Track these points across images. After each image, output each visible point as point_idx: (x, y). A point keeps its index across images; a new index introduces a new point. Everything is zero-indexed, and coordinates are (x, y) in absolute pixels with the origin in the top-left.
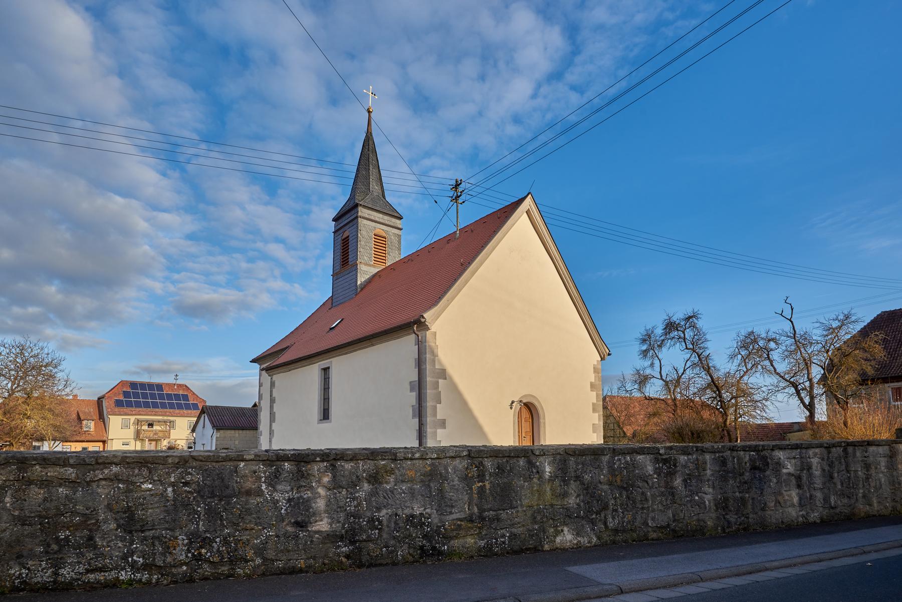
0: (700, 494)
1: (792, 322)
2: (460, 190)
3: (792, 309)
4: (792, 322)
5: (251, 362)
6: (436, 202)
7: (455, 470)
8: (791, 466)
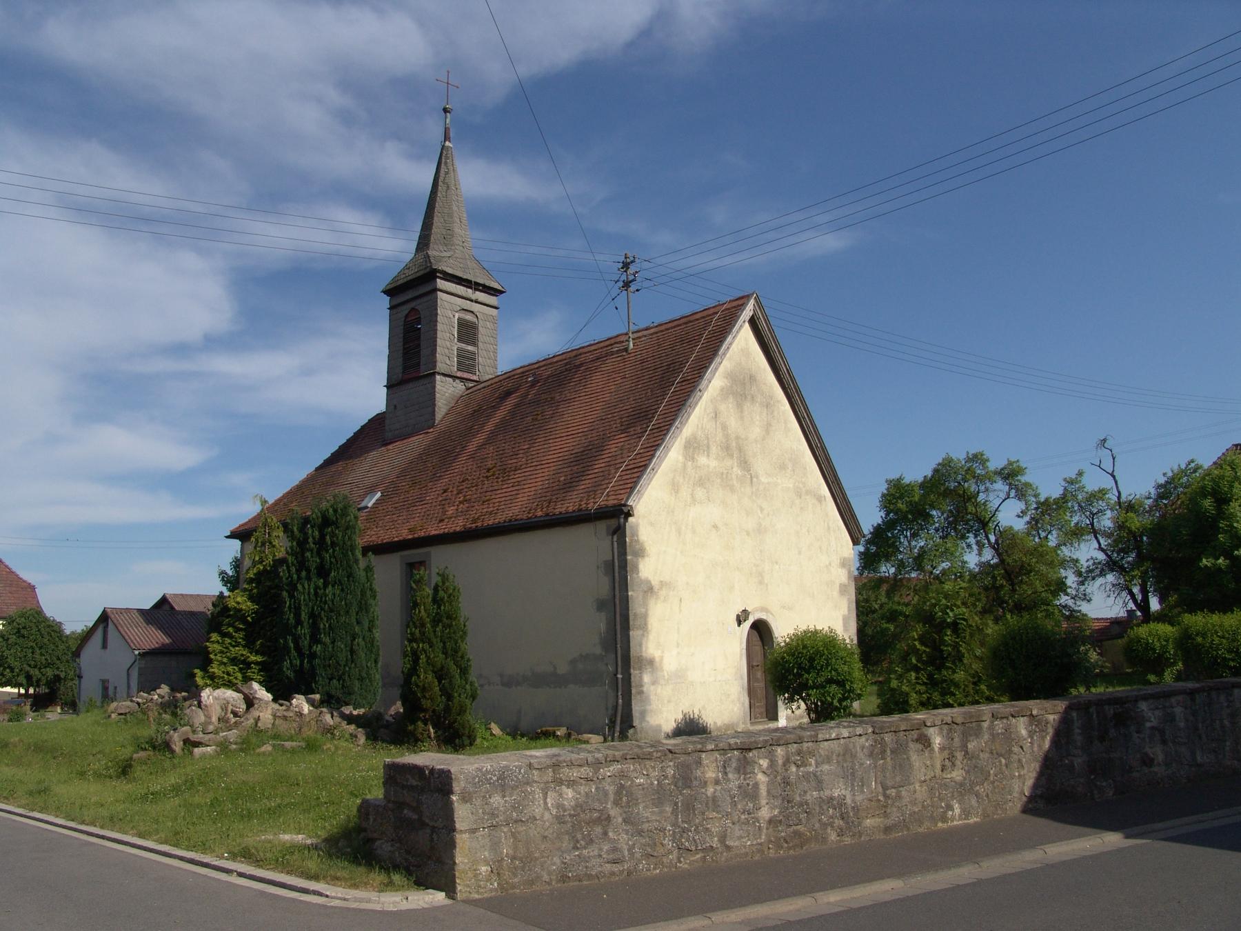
0: (1069, 758)
1: (1114, 477)
2: (632, 270)
3: (1114, 459)
4: (1114, 477)
5: (227, 537)
6: (617, 309)
7: (863, 748)
8: (1155, 718)
